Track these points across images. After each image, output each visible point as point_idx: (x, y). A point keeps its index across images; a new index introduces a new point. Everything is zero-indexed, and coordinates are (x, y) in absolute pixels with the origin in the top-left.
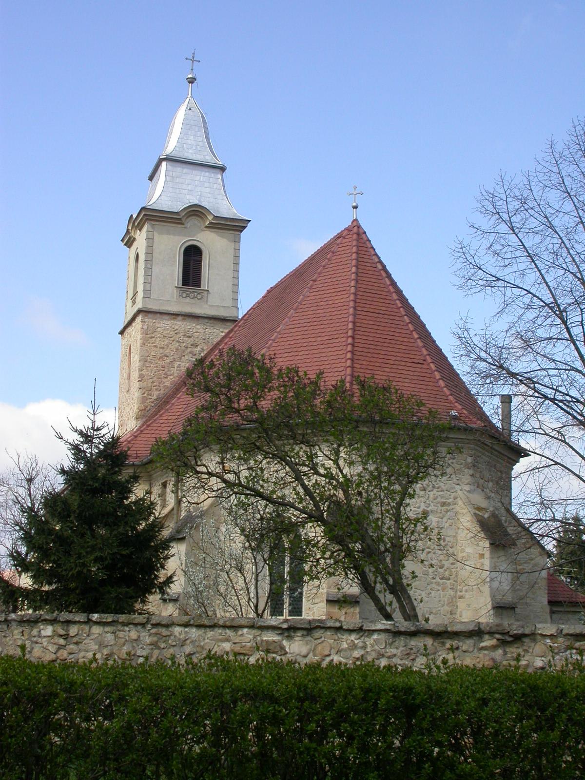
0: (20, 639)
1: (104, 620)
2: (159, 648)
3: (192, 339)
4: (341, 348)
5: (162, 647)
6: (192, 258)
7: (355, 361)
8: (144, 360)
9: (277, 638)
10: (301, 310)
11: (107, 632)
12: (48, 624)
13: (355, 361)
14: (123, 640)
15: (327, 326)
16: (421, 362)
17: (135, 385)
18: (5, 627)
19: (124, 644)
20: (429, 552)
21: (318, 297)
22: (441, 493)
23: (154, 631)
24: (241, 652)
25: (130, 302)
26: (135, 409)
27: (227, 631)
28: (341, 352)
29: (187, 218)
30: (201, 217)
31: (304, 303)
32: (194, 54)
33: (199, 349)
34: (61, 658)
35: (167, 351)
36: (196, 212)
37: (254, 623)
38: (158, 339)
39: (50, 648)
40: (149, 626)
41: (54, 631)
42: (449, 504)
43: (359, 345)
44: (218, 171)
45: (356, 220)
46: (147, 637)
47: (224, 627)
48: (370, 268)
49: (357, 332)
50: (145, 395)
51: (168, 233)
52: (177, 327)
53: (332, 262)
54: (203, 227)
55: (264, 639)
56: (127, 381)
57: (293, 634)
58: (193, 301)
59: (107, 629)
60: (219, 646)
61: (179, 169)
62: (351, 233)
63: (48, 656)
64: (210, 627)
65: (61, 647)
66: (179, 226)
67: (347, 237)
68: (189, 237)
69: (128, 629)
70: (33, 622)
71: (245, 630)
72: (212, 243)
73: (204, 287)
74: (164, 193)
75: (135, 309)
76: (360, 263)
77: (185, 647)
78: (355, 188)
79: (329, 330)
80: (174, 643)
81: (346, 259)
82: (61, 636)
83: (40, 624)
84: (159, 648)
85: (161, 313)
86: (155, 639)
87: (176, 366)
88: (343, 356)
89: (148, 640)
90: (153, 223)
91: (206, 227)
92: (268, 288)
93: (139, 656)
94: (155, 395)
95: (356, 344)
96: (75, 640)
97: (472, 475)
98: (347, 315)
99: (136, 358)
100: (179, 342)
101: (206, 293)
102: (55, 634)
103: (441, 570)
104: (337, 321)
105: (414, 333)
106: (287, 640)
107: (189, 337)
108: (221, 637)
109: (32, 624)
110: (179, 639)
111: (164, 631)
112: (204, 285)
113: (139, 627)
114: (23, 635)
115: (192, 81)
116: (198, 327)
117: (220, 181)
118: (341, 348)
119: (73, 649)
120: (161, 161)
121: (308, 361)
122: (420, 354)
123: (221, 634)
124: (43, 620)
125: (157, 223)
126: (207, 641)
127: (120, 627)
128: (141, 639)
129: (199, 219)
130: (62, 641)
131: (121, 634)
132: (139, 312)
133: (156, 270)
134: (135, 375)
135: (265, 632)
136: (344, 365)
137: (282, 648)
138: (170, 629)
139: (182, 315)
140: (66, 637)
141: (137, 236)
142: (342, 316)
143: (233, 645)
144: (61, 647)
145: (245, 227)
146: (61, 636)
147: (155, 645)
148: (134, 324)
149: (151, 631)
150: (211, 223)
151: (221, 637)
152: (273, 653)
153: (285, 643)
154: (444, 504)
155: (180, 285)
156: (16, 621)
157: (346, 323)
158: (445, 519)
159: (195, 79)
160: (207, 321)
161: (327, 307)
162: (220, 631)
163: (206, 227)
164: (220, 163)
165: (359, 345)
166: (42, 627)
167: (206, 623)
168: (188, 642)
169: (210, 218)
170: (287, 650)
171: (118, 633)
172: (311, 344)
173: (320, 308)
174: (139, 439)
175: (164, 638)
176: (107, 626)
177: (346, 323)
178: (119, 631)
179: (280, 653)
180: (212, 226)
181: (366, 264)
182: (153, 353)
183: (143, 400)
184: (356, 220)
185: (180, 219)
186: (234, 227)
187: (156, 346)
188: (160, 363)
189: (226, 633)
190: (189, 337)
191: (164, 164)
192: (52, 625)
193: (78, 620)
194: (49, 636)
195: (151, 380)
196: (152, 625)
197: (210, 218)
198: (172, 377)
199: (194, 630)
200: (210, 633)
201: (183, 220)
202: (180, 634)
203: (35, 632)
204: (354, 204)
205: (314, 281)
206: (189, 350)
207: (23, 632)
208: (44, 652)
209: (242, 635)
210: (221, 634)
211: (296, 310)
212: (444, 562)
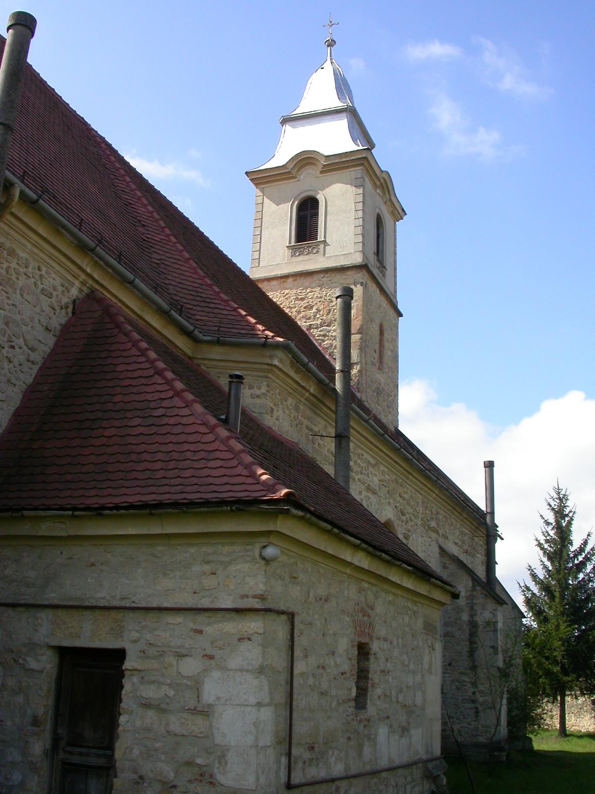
29: (299, 170)
30: (310, 164)
33: (314, 310)
36: (305, 160)
58: (307, 257)
91: (322, 172)
107: (302, 299)
112: (320, 237)
129: (313, 167)
160: (322, 275)
190: (302, 299)
201: (294, 172)
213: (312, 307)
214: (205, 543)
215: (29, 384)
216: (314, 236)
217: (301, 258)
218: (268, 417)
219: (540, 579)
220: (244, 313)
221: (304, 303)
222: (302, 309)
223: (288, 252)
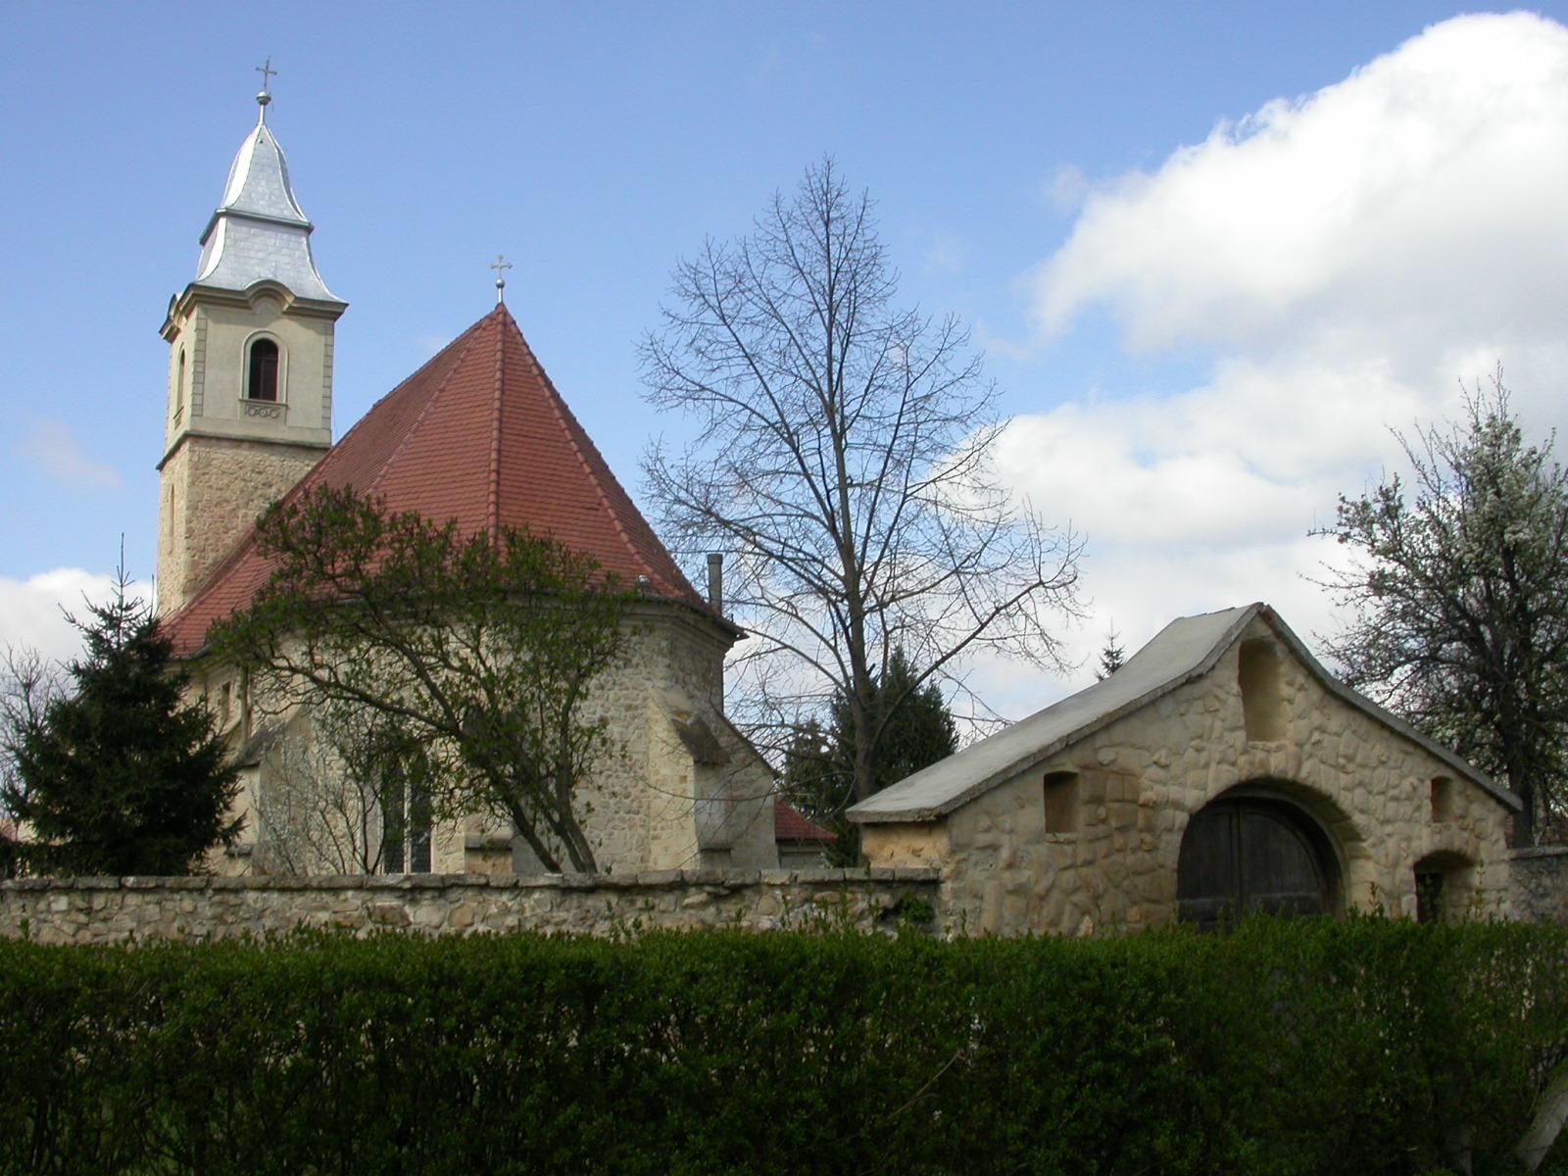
3: (263, 476)
6: (264, 355)
9: (395, 903)
12: (60, 894)
17: (181, 543)
20: (609, 776)
22: (625, 692)
23: (217, 898)
27: (324, 895)
30: (275, 298)
31: (426, 422)
36: (269, 291)
41: (70, 904)
42: (636, 708)
44: (303, 232)
45: (501, 304)
47: (320, 889)
51: (229, 322)
54: (279, 314)
56: (169, 538)
59: (148, 898)
65: (81, 927)
68: (254, 325)
70: (37, 891)
71: (350, 894)
73: (281, 399)
78: (501, 258)
80: (247, 916)
82: (80, 910)
84: (225, 923)
87: (240, 515)
88: (484, 499)
90: (207, 306)
91: (285, 313)
92: (375, 401)
96: (101, 915)
97: (669, 666)
99: (181, 504)
101: (284, 409)
102: (72, 908)
103: (628, 801)
107: (260, 473)
108: (314, 904)
109: (38, 894)
110: (254, 909)
111: (232, 899)
112: (281, 398)
115: (264, 101)
116: (273, 458)
124: (52, 889)
125: (212, 307)
127: (167, 895)
129: (273, 301)
130: (82, 918)
131: (169, 905)
140: (88, 911)
141: (181, 327)
145: (340, 314)
146: (80, 910)
148: (178, 455)
150: (290, 307)
154: (629, 708)
155: (246, 398)
158: (631, 728)
162: (313, 896)
163: (285, 313)
166: (52, 898)
168: (268, 912)
169: (290, 300)
183: (193, 565)
184: (501, 304)
185: (246, 301)
187: (210, 487)
190: (260, 473)
192: (67, 894)
196: (215, 890)
197: (290, 300)
199: (276, 895)
200: (299, 900)
201: (251, 304)
203: (42, 905)
204: (499, 281)
206: (259, 492)
207: (24, 906)
209: (345, 900)
210: (314, 900)
212: (630, 789)
213: (271, 486)
214: (804, 853)
215: (1242, 722)
216: (271, 394)
217: (257, 419)
218: (1415, 844)
219: (81, 698)
220: (629, 545)
221: (261, 478)
222: (260, 486)
223: (239, 408)
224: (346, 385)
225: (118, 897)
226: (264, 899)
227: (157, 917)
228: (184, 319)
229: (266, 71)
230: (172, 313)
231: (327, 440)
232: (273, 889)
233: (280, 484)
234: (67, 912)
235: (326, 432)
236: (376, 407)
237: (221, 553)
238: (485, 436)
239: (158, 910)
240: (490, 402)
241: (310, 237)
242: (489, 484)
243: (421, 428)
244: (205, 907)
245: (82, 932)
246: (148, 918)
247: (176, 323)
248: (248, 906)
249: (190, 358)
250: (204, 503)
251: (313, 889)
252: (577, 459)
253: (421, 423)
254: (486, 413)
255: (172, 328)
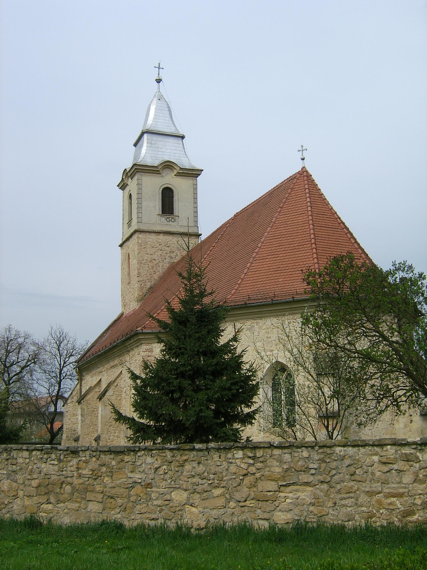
0: (219, 461)
1: (283, 445)
2: (325, 462)
4: (308, 251)
5: (328, 461)
6: (167, 195)
7: (319, 259)
8: (140, 263)
9: (412, 451)
10: (275, 227)
11: (285, 454)
13: (319, 259)
14: (298, 458)
15: (296, 237)
16: (359, 258)
17: (135, 280)
18: (206, 453)
19: (298, 461)
21: (286, 218)
24: (387, 462)
25: (126, 226)
26: (136, 295)
27: (375, 448)
28: (308, 254)
30: (171, 169)
31: (277, 222)
32: (159, 64)
34: (252, 472)
35: (155, 257)
36: (168, 165)
37: (395, 442)
38: (148, 249)
39: (242, 466)
40: (317, 447)
41: (244, 454)
43: (320, 248)
44: (180, 139)
45: (304, 167)
46: (316, 455)
47: (373, 445)
48: (317, 198)
49: (317, 240)
50: (142, 285)
52: (160, 241)
53: (292, 195)
55: (403, 452)
56: (127, 277)
57: (424, 448)
59: (286, 451)
60: (369, 459)
61: (155, 137)
62: (302, 176)
63: (241, 472)
64: (362, 446)
65: (250, 465)
66: (158, 175)
67: (299, 179)
69: (301, 451)
70: (227, 449)
71: (389, 447)
72: (180, 186)
74: (148, 154)
75: (132, 230)
76: (311, 195)
77: (345, 461)
78: (302, 146)
79: (297, 239)
80: (336, 459)
81: (301, 193)
82: (250, 457)
83: (233, 450)
84: (325, 462)
85: (150, 232)
86: (322, 456)
87: (161, 266)
88: (311, 256)
89: (316, 457)
91: (175, 175)
92: (235, 214)
93: (311, 468)
94: (149, 285)
95: (318, 248)
96: (261, 459)
98: (308, 229)
99: (134, 262)
100: (161, 250)
101: (177, 217)
102: (245, 456)
104: (302, 233)
105: (351, 239)
106: (420, 453)
107: (168, 247)
108: (370, 453)
109: (227, 451)
110: (340, 455)
111: (328, 451)
113: (309, 449)
114: (220, 458)
117: (181, 145)
118: (308, 251)
119: (260, 466)
120: (143, 133)
121: (286, 260)
122: (357, 253)
123: (371, 450)
124: (235, 447)
125: (144, 174)
126: (360, 456)
127: (295, 449)
128: (312, 456)
130: (251, 461)
131: (296, 454)
132: (135, 232)
133: (144, 204)
134: (134, 273)
135: (404, 448)
136: (312, 262)
137: (417, 458)
138: (333, 449)
139: (163, 233)
140: (254, 458)
141: (129, 183)
142: (305, 230)
143: (381, 458)
144: (250, 465)
145: (200, 174)
146: (250, 457)
147: (322, 461)
148: (131, 240)
149: (319, 451)
151: (370, 453)
152: (411, 461)
153: (418, 454)
155: (161, 213)
156: (214, 448)
157: (309, 235)
159: (161, 80)
161: (294, 224)
162: (370, 448)
164: (181, 133)
165: (320, 248)
166: (235, 452)
167: (359, 443)
168: (347, 457)
170: (421, 459)
171: (293, 453)
172: (287, 249)
173: (289, 225)
174: (160, 315)
175: (328, 455)
176: (285, 449)
177: (309, 235)
178: (294, 452)
179: (416, 461)
180: (179, 175)
181: (315, 196)
182: (146, 258)
183: (141, 288)
184: (304, 167)
186: (193, 174)
187: (147, 254)
188: (151, 264)
189: (374, 450)
190: (168, 247)
191: (145, 136)
192: (242, 450)
193: (262, 446)
194: (241, 458)
195: (146, 276)
196: (319, 447)
198: (158, 273)
199: (350, 448)
200: (362, 450)
201: (161, 171)
202: (340, 452)
203: (230, 455)
204: (302, 157)
205: (281, 208)
206: (169, 255)
207: (220, 456)
208: (238, 469)
209: (387, 450)
210: (371, 450)
211: (272, 227)
222: (168, 252)
224: (214, 208)
225: (269, 451)
226: (345, 451)
227: (290, 460)
228: (130, 179)
229: (159, 68)
230: (124, 178)
231: (197, 231)
232: (348, 446)
233: (177, 251)
234: (243, 458)
235: (196, 227)
236: (236, 215)
237: (153, 283)
238: (306, 227)
239: (290, 457)
240: (306, 212)
241: (184, 140)
242: (312, 249)
243: (275, 225)
244: (314, 454)
245: (250, 468)
246: (285, 461)
247: (126, 182)
248: (337, 454)
249: (134, 197)
250: (145, 261)
251: (369, 445)
252: (348, 237)
253: (274, 223)
254: (305, 217)
255: (124, 184)
